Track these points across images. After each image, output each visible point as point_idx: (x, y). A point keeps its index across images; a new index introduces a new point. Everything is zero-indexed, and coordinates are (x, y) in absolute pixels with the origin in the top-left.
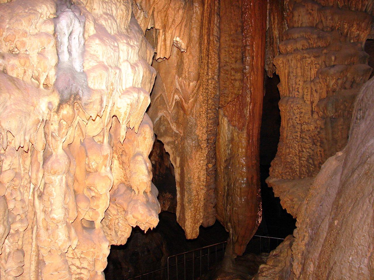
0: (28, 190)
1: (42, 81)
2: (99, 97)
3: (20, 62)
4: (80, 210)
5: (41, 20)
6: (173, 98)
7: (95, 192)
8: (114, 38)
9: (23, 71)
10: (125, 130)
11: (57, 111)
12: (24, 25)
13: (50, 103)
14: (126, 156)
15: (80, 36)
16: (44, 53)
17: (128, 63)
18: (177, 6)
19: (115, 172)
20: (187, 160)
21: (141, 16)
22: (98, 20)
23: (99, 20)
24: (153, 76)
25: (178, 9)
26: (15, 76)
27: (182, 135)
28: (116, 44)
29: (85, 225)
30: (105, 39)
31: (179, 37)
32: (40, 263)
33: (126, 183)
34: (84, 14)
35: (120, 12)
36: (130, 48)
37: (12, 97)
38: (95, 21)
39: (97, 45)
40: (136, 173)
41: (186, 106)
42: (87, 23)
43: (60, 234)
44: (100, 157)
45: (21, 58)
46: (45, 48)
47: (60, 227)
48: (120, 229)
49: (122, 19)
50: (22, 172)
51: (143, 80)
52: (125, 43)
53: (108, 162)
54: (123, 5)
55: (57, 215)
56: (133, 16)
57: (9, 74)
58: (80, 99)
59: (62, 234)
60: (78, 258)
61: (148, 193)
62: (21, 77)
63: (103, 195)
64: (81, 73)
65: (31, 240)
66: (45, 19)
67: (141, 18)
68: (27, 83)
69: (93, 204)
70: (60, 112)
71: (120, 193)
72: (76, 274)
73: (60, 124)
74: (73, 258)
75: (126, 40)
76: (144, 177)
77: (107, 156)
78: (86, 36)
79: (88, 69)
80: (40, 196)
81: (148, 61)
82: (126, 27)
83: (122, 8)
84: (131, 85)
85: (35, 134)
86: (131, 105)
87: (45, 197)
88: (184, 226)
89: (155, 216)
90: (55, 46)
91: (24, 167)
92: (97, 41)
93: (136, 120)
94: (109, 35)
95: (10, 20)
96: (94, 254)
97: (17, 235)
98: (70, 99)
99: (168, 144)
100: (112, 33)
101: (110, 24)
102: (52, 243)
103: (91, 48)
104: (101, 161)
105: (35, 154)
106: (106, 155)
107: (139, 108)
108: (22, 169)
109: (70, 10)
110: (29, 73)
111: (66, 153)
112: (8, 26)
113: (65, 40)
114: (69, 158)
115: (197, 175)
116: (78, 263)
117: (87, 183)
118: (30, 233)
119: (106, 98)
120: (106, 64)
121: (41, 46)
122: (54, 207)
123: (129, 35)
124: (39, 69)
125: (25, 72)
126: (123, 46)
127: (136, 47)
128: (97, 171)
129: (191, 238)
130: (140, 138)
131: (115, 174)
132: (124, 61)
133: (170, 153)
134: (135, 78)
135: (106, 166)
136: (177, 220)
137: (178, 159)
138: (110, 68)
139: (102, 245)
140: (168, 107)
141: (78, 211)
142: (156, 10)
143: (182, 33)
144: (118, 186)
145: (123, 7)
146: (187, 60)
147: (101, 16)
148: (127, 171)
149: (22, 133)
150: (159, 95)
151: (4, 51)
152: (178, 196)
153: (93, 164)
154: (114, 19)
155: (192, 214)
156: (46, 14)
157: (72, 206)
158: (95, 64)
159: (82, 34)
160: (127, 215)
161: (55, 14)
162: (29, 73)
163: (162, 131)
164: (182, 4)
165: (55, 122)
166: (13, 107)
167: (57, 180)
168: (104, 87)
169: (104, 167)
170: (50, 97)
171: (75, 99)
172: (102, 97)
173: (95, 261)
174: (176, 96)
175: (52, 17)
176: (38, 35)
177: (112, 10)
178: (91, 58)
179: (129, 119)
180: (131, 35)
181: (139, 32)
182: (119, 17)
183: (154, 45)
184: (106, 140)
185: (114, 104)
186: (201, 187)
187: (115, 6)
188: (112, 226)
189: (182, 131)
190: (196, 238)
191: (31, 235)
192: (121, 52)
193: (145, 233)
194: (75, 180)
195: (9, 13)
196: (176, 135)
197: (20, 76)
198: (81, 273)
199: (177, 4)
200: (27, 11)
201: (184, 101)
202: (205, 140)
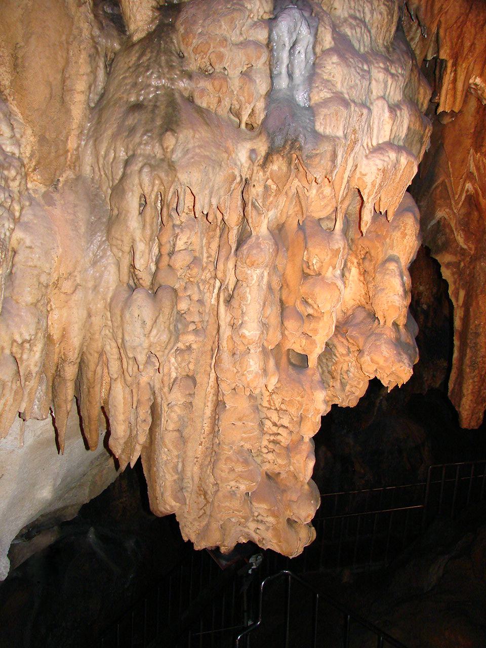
0: (211, 288)
1: (245, 118)
2: (330, 148)
3: (213, 85)
4: (286, 332)
5: (250, 21)
7: (313, 308)
8: (364, 58)
9: (217, 99)
10: (371, 212)
11: (264, 166)
12: (223, 28)
13: (253, 151)
14: (371, 261)
15: (308, 50)
16: (250, 74)
19: (351, 287)
20: (477, 296)
21: (416, 37)
22: (339, 27)
23: (341, 26)
24: (427, 131)
26: (204, 105)
27: (472, 252)
28: (365, 67)
29: (292, 360)
30: (347, 56)
31: (481, 76)
32: (219, 405)
33: (367, 307)
34: (317, 15)
35: (376, 16)
36: (389, 77)
37: (197, 136)
38: (334, 28)
39: (335, 66)
40: (383, 289)
42: (321, 29)
43: (252, 363)
44: (326, 250)
45: (215, 79)
46: (252, 66)
47: (252, 351)
48: (350, 382)
49: (379, 29)
50: (205, 260)
51: (410, 136)
52: (382, 68)
53: (339, 265)
54: (384, 4)
55: (249, 332)
56: (399, 28)
57: (197, 104)
58: (300, 149)
59: (254, 363)
60: (276, 409)
61: (401, 326)
62: (213, 107)
63: (325, 314)
64: (305, 108)
65: (208, 369)
66: (255, 19)
67: (417, 39)
68: (222, 119)
69: (308, 327)
70: (267, 166)
71: (357, 322)
72: (270, 435)
73: (266, 188)
74: (269, 409)
75: (384, 64)
77: (338, 251)
78: (318, 50)
79: (317, 102)
80: (229, 300)
81: (420, 107)
82: (385, 44)
83: (382, 10)
84: (387, 139)
85: (226, 197)
86: (384, 171)
87: (235, 303)
89: (407, 364)
90: (268, 63)
91: (208, 252)
92: (335, 59)
93: (390, 199)
94: (355, 53)
95: (204, 20)
96: (301, 405)
97: (187, 352)
98: (284, 147)
99: (448, 265)
100: (362, 50)
101: (359, 35)
102: (238, 375)
103: (323, 69)
104: (327, 259)
105: (226, 233)
106: (337, 249)
107: (397, 180)
108: (205, 255)
109: (296, 7)
110: (226, 103)
111: (273, 236)
112: (200, 31)
113: (285, 55)
114: (276, 244)
116: (275, 417)
117: (301, 291)
118: (209, 357)
119: (342, 152)
120: (346, 96)
121: (247, 62)
122: (246, 318)
123: (390, 56)
124: (242, 98)
125: (219, 101)
126: (378, 75)
127: (401, 78)
128: (320, 274)
130: (397, 235)
131: (351, 292)
132: (378, 98)
133: (450, 281)
134: (395, 128)
135: (334, 268)
136: (449, 394)
137: (462, 294)
138: (353, 105)
139: (315, 394)
140: (453, 202)
141: (283, 334)
142: (443, 26)
144: (354, 310)
145: (383, 8)
147: (346, 20)
148: (370, 286)
149: (207, 192)
150: (439, 181)
151: (193, 68)
152: (456, 355)
153: (314, 262)
154: (366, 26)
155: (474, 387)
156: (258, 12)
157: (274, 320)
158: (329, 96)
159: (311, 46)
160: (362, 356)
161: (271, 12)
162: (226, 103)
163: (440, 244)
165: (259, 182)
166: (197, 151)
167: (255, 277)
168: (340, 134)
169: (331, 269)
170: (254, 142)
171: (292, 147)
172: (335, 149)
173: (302, 419)
174: (469, 186)
175: (266, 17)
176: (244, 44)
177: (364, 13)
178: (323, 85)
180: (395, 57)
181: (408, 55)
182: (375, 25)
183: (436, 89)
184: (339, 226)
185: (356, 166)
187: (370, 7)
188: (338, 373)
189: (473, 247)
190: (476, 428)
192: (374, 82)
193: (389, 392)
194: (284, 284)
195: (204, 11)
197: (212, 107)
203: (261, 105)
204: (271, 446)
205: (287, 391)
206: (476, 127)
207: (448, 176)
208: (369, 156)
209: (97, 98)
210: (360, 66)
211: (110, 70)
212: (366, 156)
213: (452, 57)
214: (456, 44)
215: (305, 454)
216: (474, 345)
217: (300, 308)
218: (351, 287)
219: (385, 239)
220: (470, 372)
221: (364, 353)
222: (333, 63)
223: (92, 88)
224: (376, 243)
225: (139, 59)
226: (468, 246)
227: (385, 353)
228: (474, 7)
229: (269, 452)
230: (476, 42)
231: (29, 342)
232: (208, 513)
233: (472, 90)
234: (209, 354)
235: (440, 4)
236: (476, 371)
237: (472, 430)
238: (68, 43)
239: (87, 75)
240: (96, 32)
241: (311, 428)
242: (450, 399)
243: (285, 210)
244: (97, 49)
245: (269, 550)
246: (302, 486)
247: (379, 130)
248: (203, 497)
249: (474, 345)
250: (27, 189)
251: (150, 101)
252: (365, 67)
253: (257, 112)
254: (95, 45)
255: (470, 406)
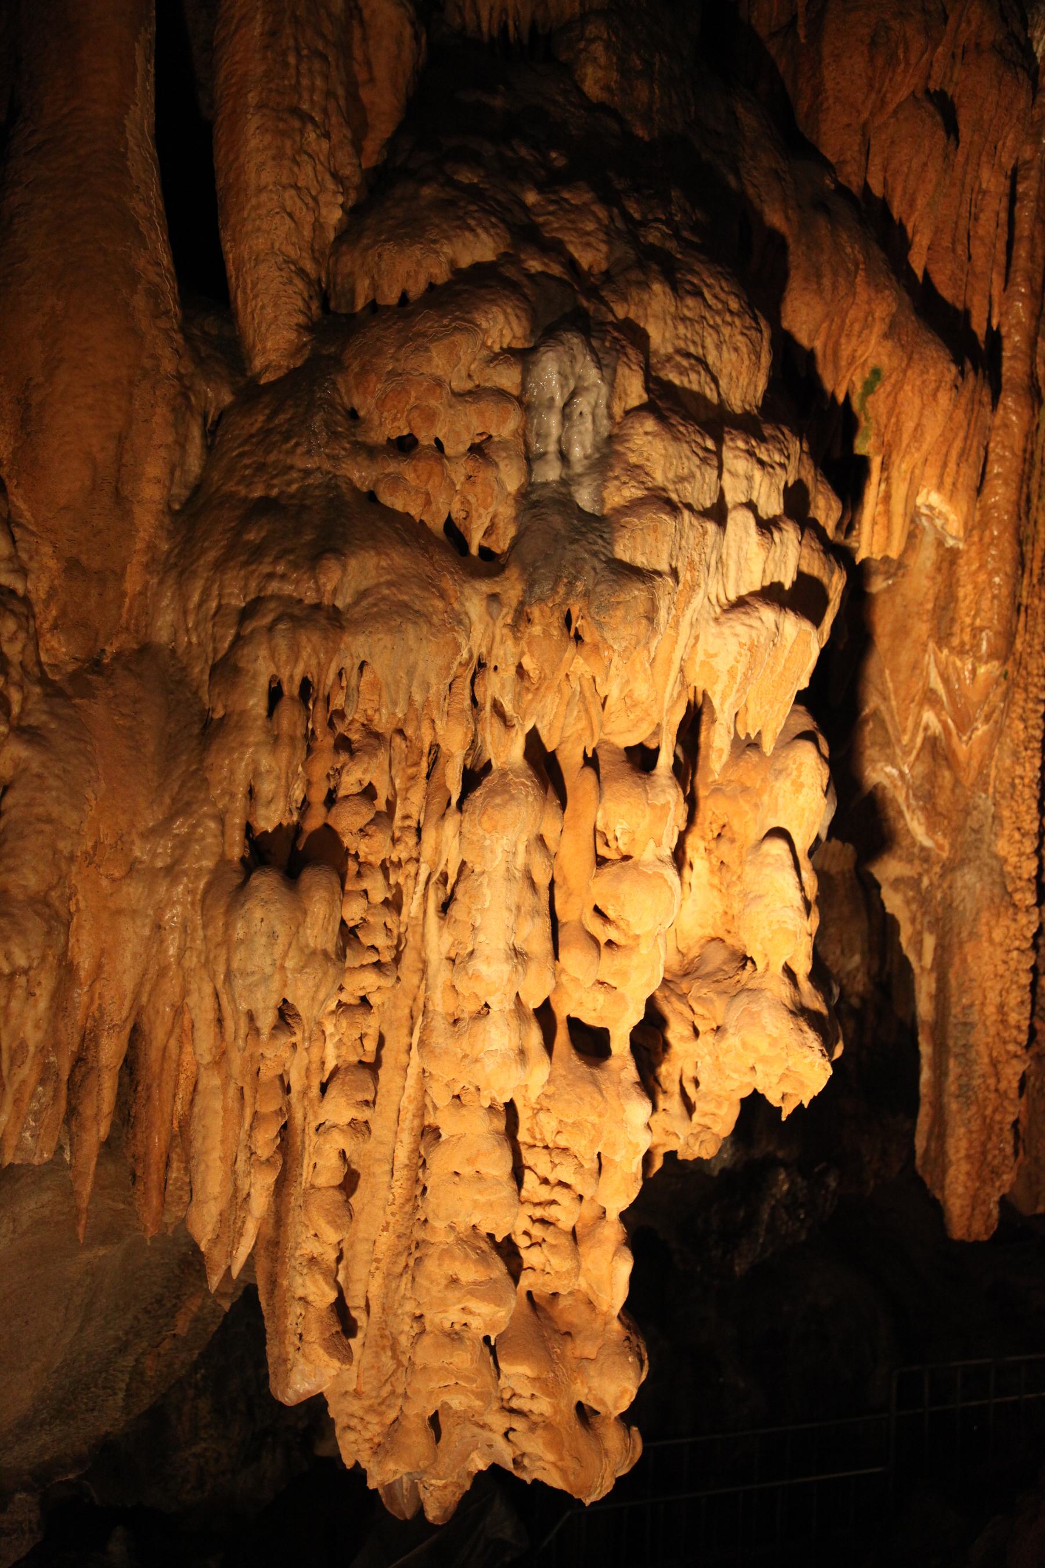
6: (917, 724)
14: (733, 841)
17: (750, 516)
18: (932, 376)
25: (933, 385)
27: (945, 855)
31: (940, 487)
33: (729, 940)
39: (650, 438)
40: (760, 897)
41: (962, 749)
60: (546, 1147)
69: (608, 966)
76: (791, 913)
87: (457, 910)
88: (942, 1188)
90: (520, 431)
92: (650, 424)
95: (399, 348)
96: (599, 1132)
99: (897, 883)
104: (645, 823)
107: (779, 669)
112: (390, 367)
115: (993, 998)
118: (405, 1031)
120: (674, 496)
122: (481, 938)
129: (966, 1239)
130: (783, 786)
135: (659, 844)
136: (918, 1162)
137: (929, 942)
139: (627, 1108)
143: (948, 481)
144: (702, 947)
146: (970, 587)
147: (669, 358)
155: (971, 1142)
158: (640, 493)
164: (949, 370)
169: (652, 844)
174: (929, 716)
177: (703, 347)
179: (744, 697)
186: (1011, 1047)
189: (946, 843)
190: (985, 1238)
191: (405, 1040)
192: (726, 476)
193: (784, 1119)
196: (925, 856)
198: (553, 1202)
199: (932, 371)
200: (445, 322)
201: (954, 731)
202: (1029, 880)
203: (506, 511)
204: (537, 1231)
205: (569, 1102)
206: (937, 599)
207: (885, 699)
208: (722, 619)
209: (185, 493)
210: (699, 440)
211: (213, 441)
212: (716, 620)
213: (878, 450)
214: (886, 427)
215: (610, 1247)
216: (963, 1050)
217: (595, 926)
218: (694, 901)
219: (759, 794)
220: (959, 1111)
221: (726, 1030)
222: (646, 433)
223: (177, 474)
224: (742, 802)
225: (270, 418)
226: (936, 843)
227: (771, 1030)
228: (916, 356)
229: (532, 1245)
230: (925, 421)
231: (25, 972)
232: (400, 1390)
233: (924, 519)
234: (407, 1024)
235: (850, 349)
236: (974, 1109)
237: (977, 1244)
238: (131, 382)
239: (168, 446)
240: (187, 367)
241: (620, 1192)
242: (920, 1172)
243: (558, 724)
244: (188, 399)
245: (535, 1481)
246: (606, 1324)
247: (739, 570)
248: (389, 1353)
249: (963, 1050)
250: (39, 663)
251: (292, 496)
252: (710, 444)
253: (501, 525)
254: (185, 393)
255: (966, 1187)
